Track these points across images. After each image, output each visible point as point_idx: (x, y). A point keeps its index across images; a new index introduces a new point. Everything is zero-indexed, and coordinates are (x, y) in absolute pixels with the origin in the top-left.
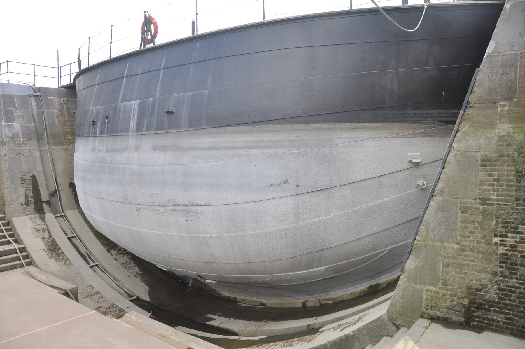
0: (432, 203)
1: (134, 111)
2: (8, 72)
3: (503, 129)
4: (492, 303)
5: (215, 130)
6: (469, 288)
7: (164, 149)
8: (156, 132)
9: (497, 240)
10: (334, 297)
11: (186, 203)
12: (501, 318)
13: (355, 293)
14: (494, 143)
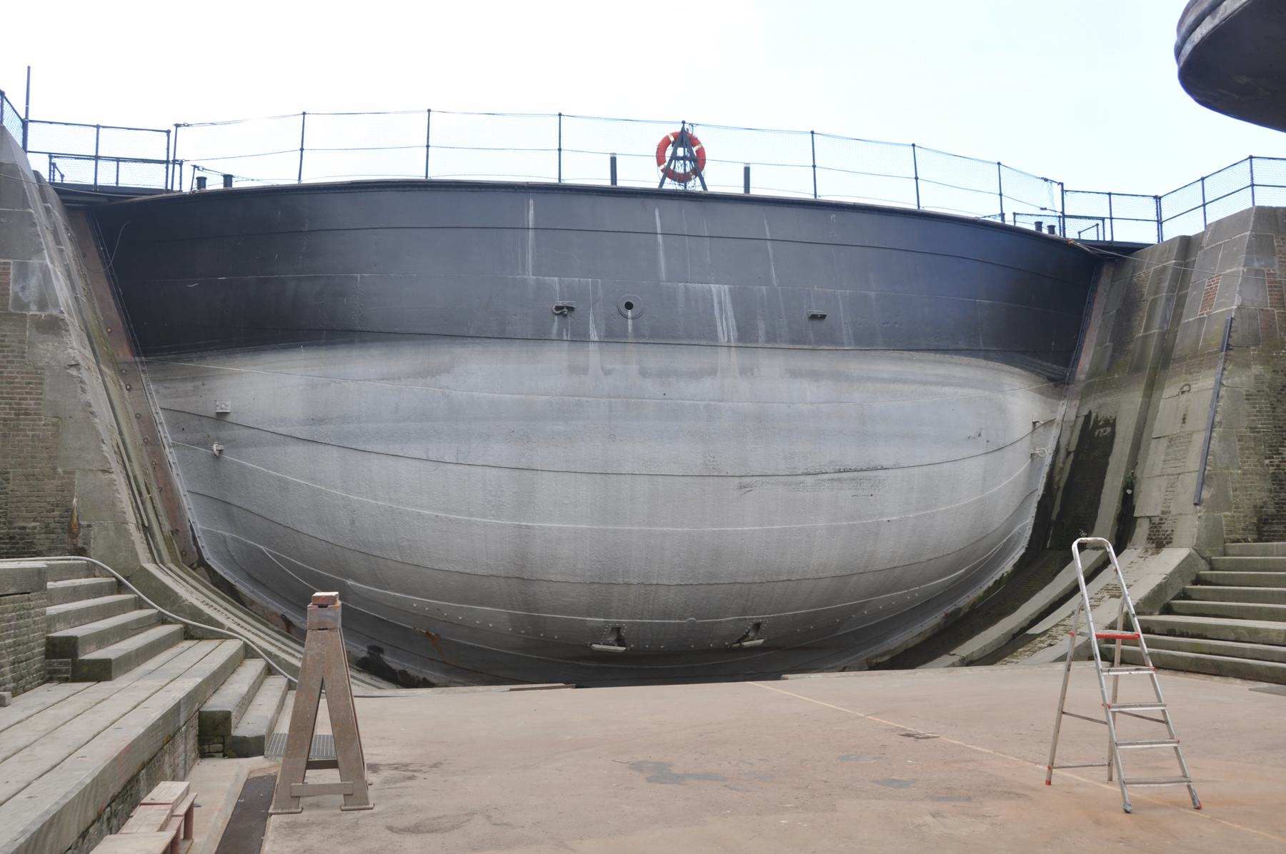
0: (1214, 434)
1: (720, 303)
2: (1253, 185)
3: (1257, 369)
4: (1273, 517)
5: (896, 354)
6: (1255, 507)
7: (815, 375)
8: (132, 416)
9: (1267, 462)
10: (892, 647)
11: (864, 466)
12: (1280, 528)
13: (925, 632)
14: (1253, 380)
